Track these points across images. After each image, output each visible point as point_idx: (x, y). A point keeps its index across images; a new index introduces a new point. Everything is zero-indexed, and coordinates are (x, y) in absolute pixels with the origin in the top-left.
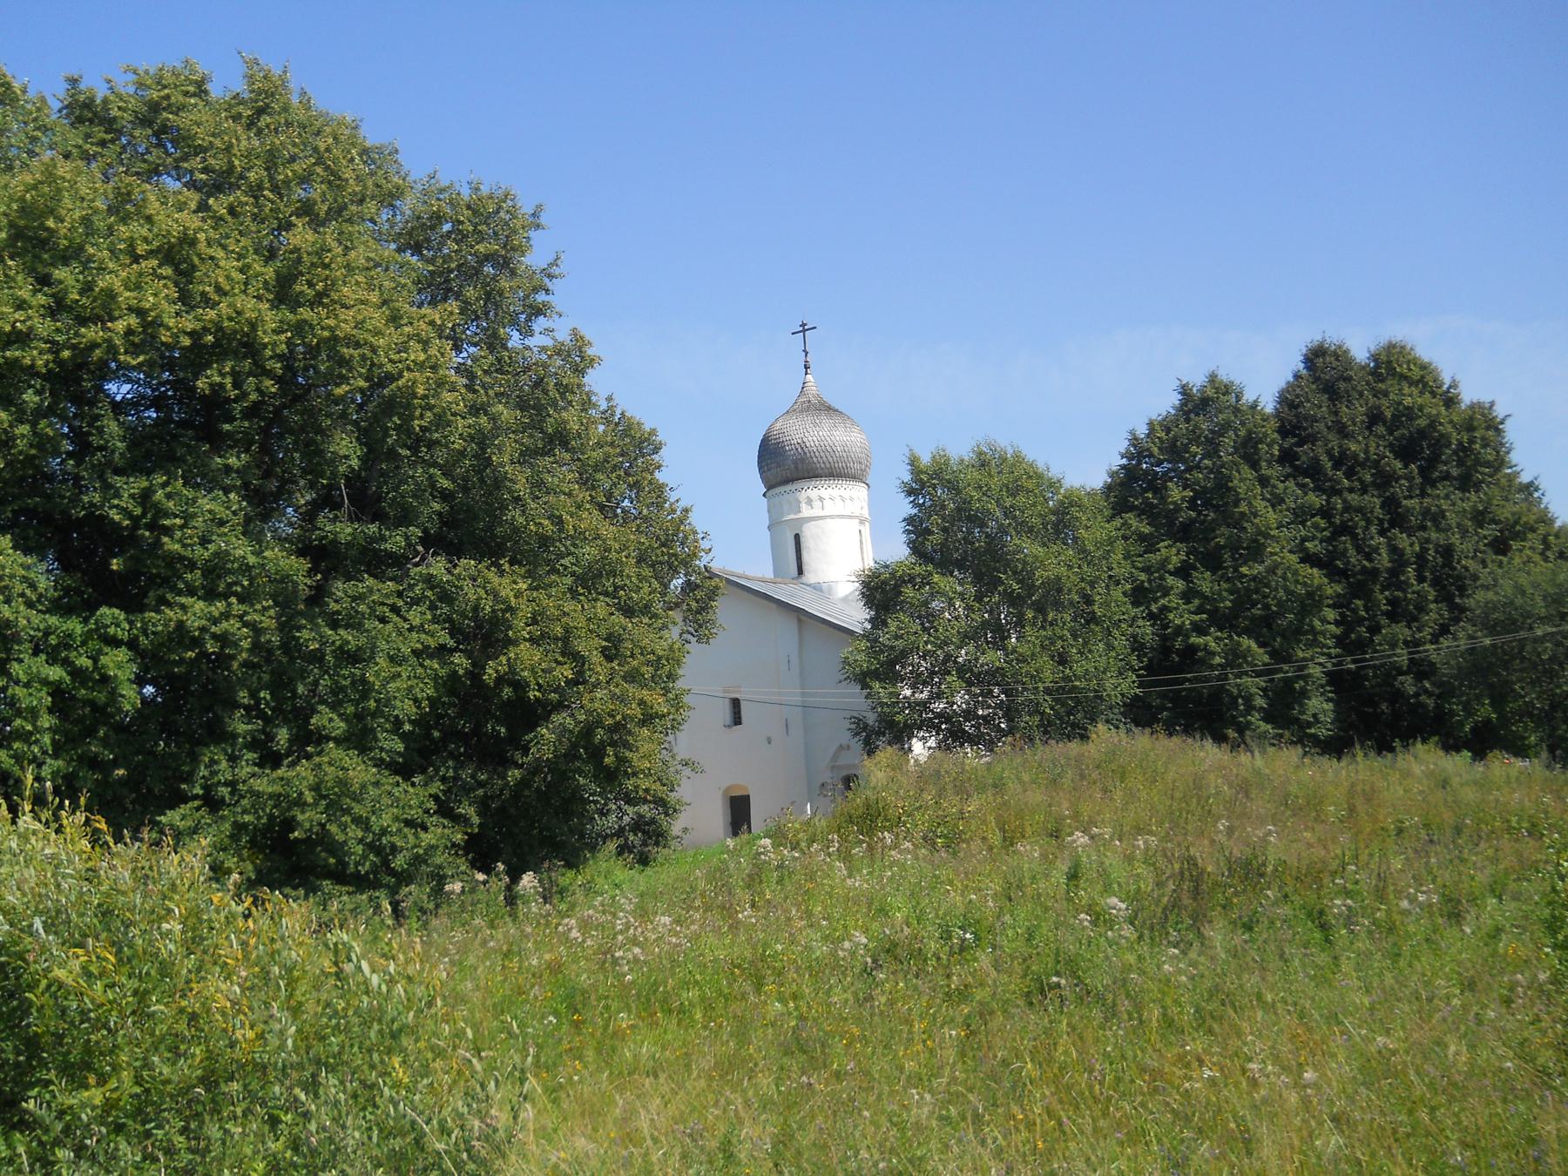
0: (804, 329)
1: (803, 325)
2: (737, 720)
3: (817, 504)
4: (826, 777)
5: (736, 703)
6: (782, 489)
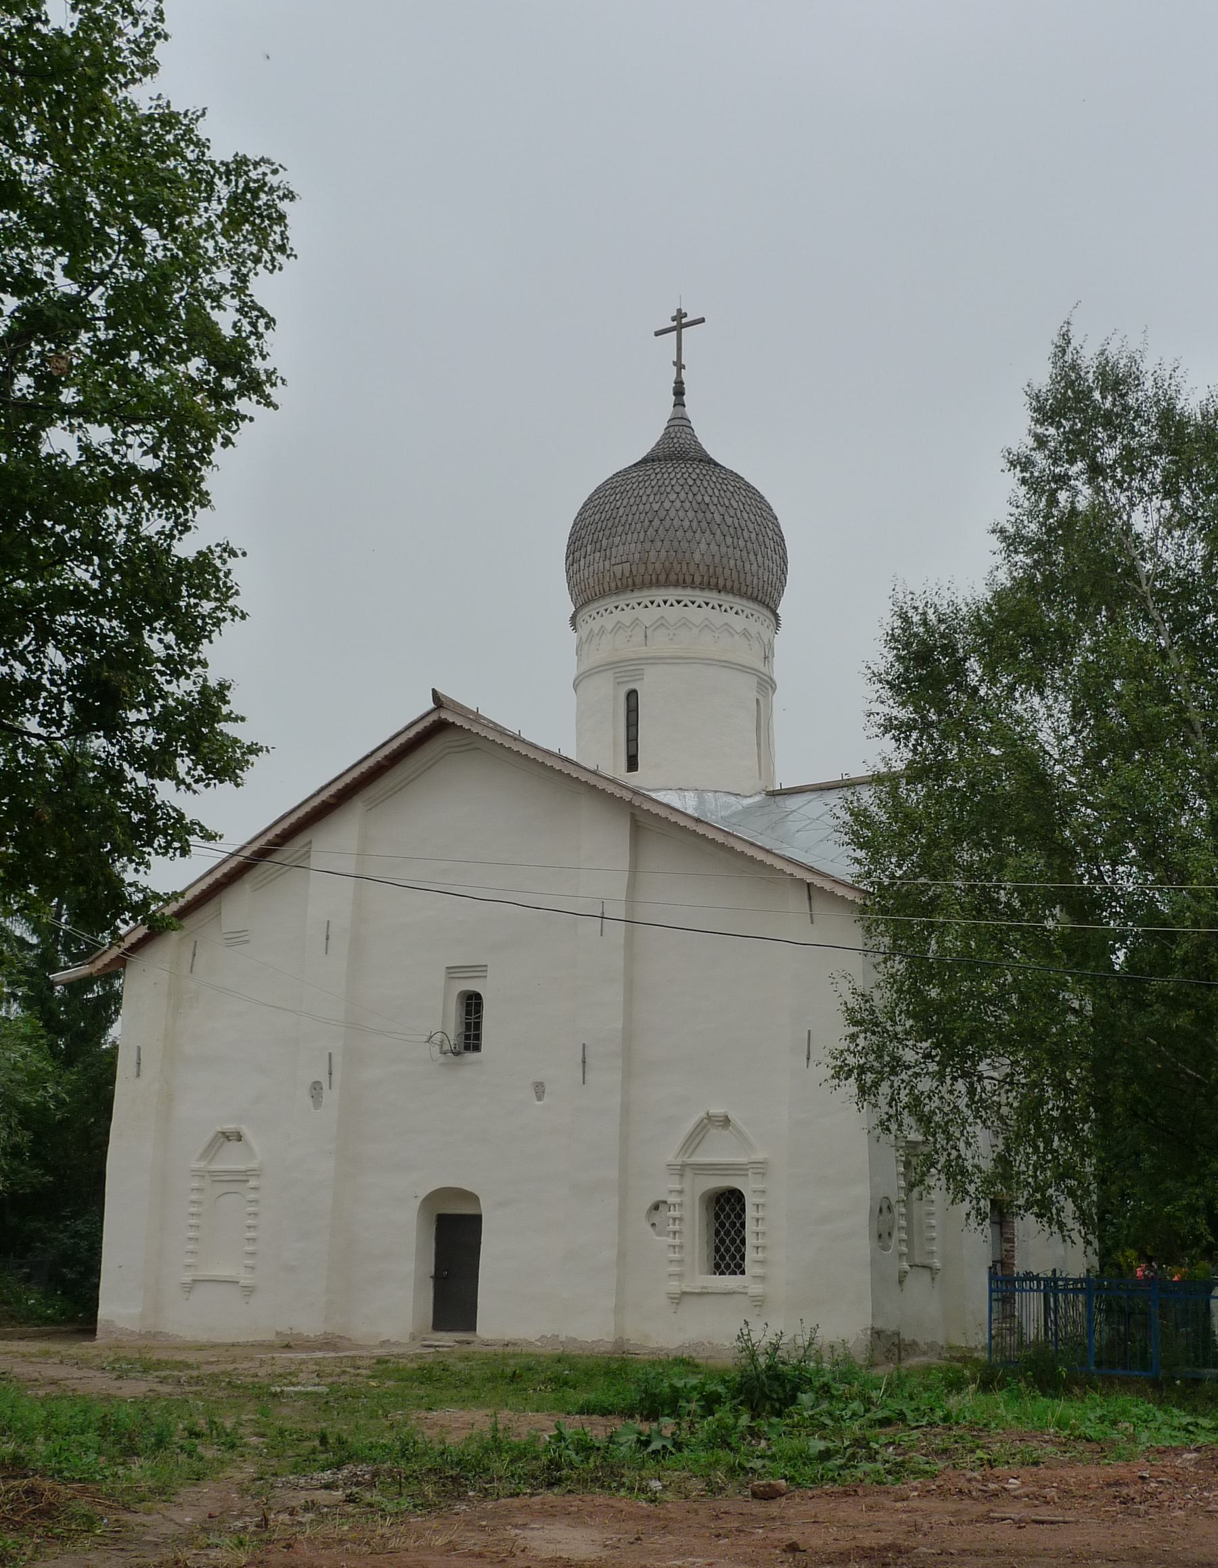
0: (680, 323)
1: (680, 315)
2: (471, 1038)
4: (664, 1187)
5: (472, 1004)
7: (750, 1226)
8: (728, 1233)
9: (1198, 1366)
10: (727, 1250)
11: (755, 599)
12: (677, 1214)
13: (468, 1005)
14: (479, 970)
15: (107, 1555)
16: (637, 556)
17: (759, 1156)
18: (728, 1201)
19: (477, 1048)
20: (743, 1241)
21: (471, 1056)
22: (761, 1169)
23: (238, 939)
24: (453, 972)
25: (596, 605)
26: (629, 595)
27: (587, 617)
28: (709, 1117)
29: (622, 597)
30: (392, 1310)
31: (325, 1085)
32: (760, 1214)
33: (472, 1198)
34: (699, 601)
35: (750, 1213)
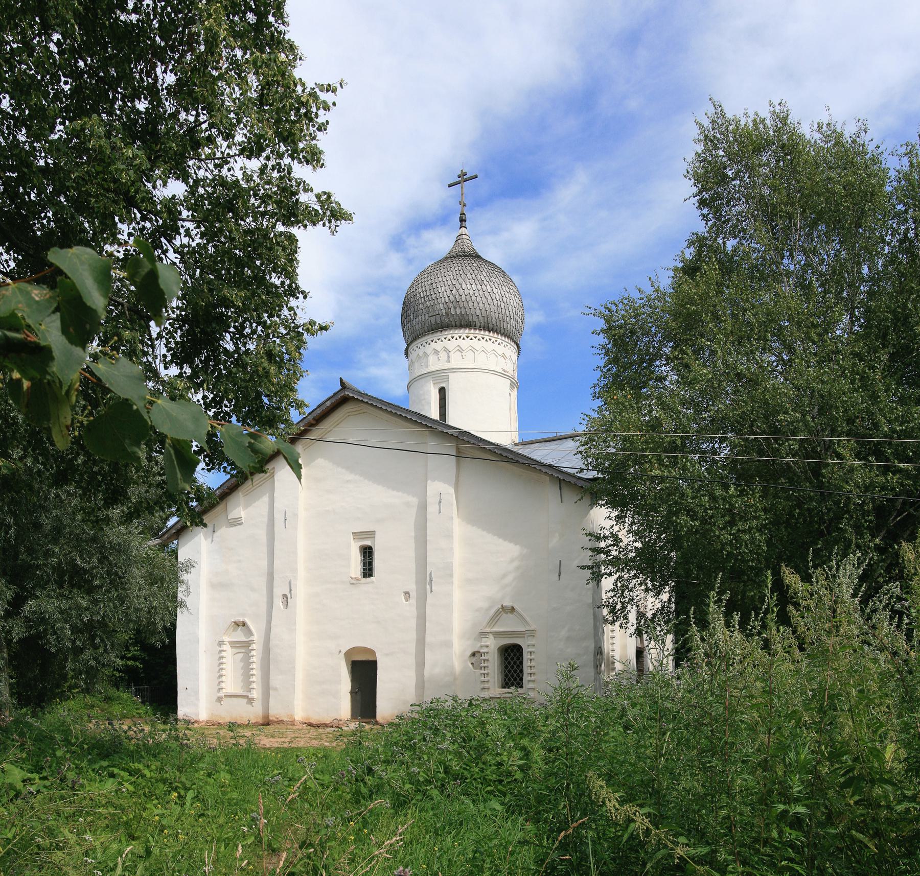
2: (368, 570)
3: (443, 355)
5: (367, 552)
6: (428, 338)
7: (526, 664)
8: (512, 667)
9: (602, 658)
10: (512, 676)
11: (508, 337)
12: (486, 658)
13: (365, 553)
14: (371, 534)
15: (293, 745)
16: (444, 311)
17: (532, 628)
18: (512, 651)
19: (371, 575)
20: (522, 671)
21: (368, 579)
22: (532, 633)
23: (237, 522)
24: (357, 535)
25: (419, 341)
26: (439, 334)
27: (415, 348)
28: (503, 607)
29: (435, 335)
30: (340, 704)
31: (289, 596)
32: (533, 657)
33: (372, 652)
34: (479, 337)
35: (526, 656)
